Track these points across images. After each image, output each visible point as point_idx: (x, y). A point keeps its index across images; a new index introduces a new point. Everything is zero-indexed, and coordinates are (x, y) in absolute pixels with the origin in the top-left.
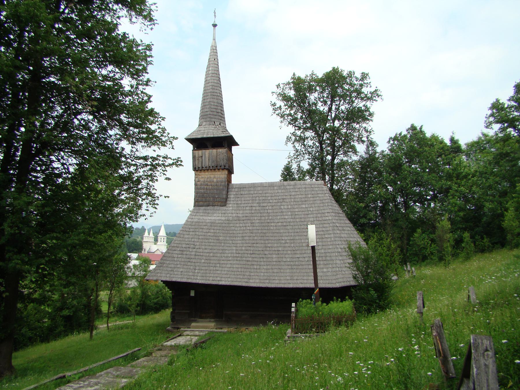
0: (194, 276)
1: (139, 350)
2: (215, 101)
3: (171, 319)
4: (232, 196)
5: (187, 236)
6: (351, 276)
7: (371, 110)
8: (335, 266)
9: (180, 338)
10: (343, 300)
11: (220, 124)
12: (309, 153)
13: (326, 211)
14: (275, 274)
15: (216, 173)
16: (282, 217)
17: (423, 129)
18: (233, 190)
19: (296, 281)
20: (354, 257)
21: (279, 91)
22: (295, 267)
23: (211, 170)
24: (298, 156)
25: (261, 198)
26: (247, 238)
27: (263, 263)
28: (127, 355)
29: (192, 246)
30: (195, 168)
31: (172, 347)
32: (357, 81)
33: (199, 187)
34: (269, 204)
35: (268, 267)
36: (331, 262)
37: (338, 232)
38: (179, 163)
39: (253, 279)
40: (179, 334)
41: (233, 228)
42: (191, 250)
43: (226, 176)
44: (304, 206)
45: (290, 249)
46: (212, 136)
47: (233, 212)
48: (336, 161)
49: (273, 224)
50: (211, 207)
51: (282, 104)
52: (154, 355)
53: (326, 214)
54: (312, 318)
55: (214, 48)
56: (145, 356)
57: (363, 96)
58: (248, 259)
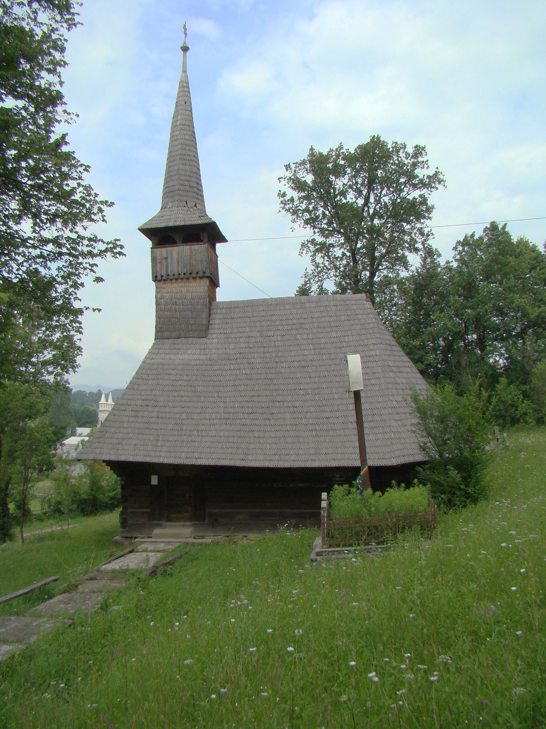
0: (155, 451)
1: (55, 580)
2: (188, 168)
3: (121, 523)
4: (216, 320)
5: (144, 387)
6: (416, 446)
7: (430, 203)
8: (388, 430)
9: (131, 555)
10: (409, 485)
11: (195, 205)
12: (336, 268)
13: (370, 342)
14: (290, 446)
15: (190, 284)
16: (300, 352)
17: (506, 230)
18: (219, 311)
19: (324, 457)
20: (423, 413)
21: (289, 174)
22: (323, 433)
23: (182, 279)
24: (319, 272)
25: (263, 324)
26: (242, 388)
27: (268, 428)
28: (31, 591)
29: (152, 402)
30: (156, 277)
31: (116, 575)
32: (407, 158)
33: (163, 307)
34: (278, 333)
35: (279, 434)
36: (382, 424)
37: (391, 375)
38: (118, 250)
39: (253, 454)
40: (130, 549)
41: (220, 372)
42: (150, 409)
43: (206, 288)
44: (334, 334)
45: (313, 403)
46: (182, 223)
47: (219, 346)
48: (376, 279)
49: (284, 365)
50: (183, 340)
51: (295, 194)
52: (80, 589)
53: (371, 347)
54: (358, 518)
55: (185, 85)
56: (64, 593)
57: (415, 181)
58: (244, 421)
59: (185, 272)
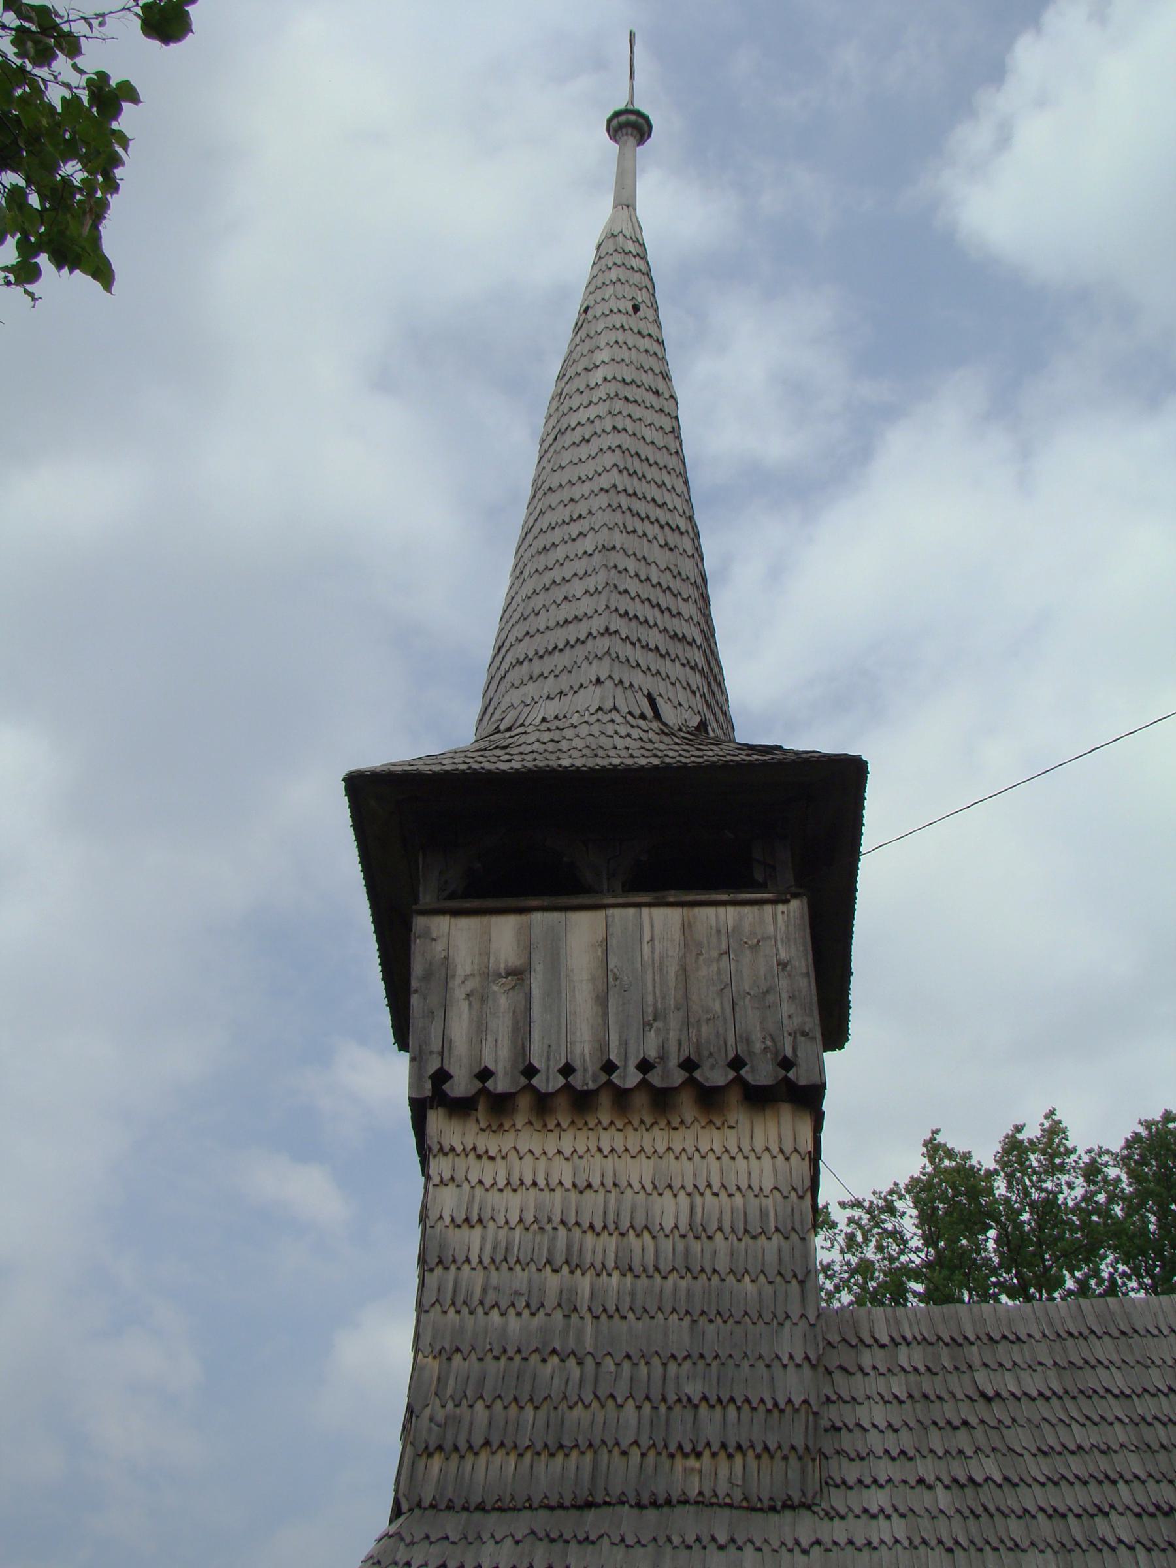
15: (682, 1140)
33: (472, 1279)
59: (652, 1054)
